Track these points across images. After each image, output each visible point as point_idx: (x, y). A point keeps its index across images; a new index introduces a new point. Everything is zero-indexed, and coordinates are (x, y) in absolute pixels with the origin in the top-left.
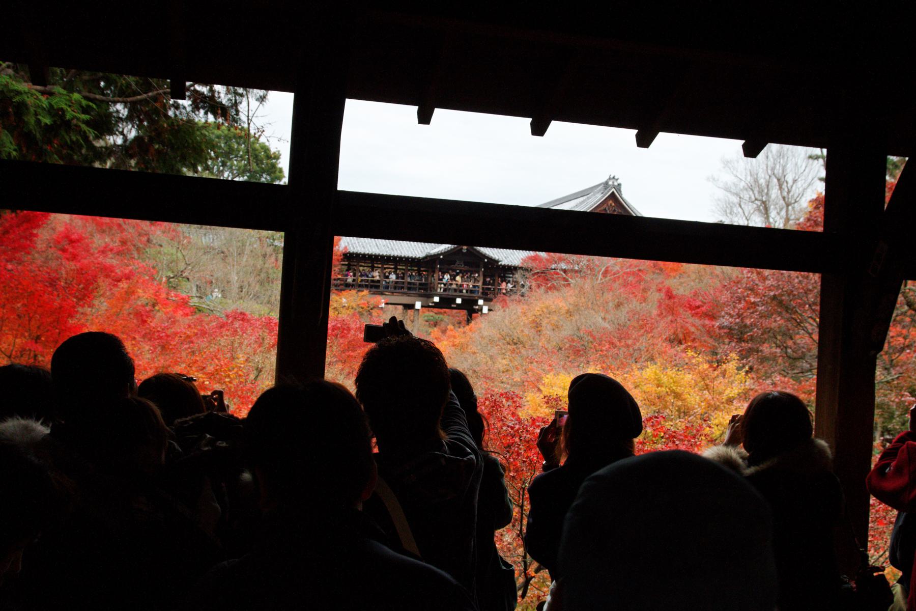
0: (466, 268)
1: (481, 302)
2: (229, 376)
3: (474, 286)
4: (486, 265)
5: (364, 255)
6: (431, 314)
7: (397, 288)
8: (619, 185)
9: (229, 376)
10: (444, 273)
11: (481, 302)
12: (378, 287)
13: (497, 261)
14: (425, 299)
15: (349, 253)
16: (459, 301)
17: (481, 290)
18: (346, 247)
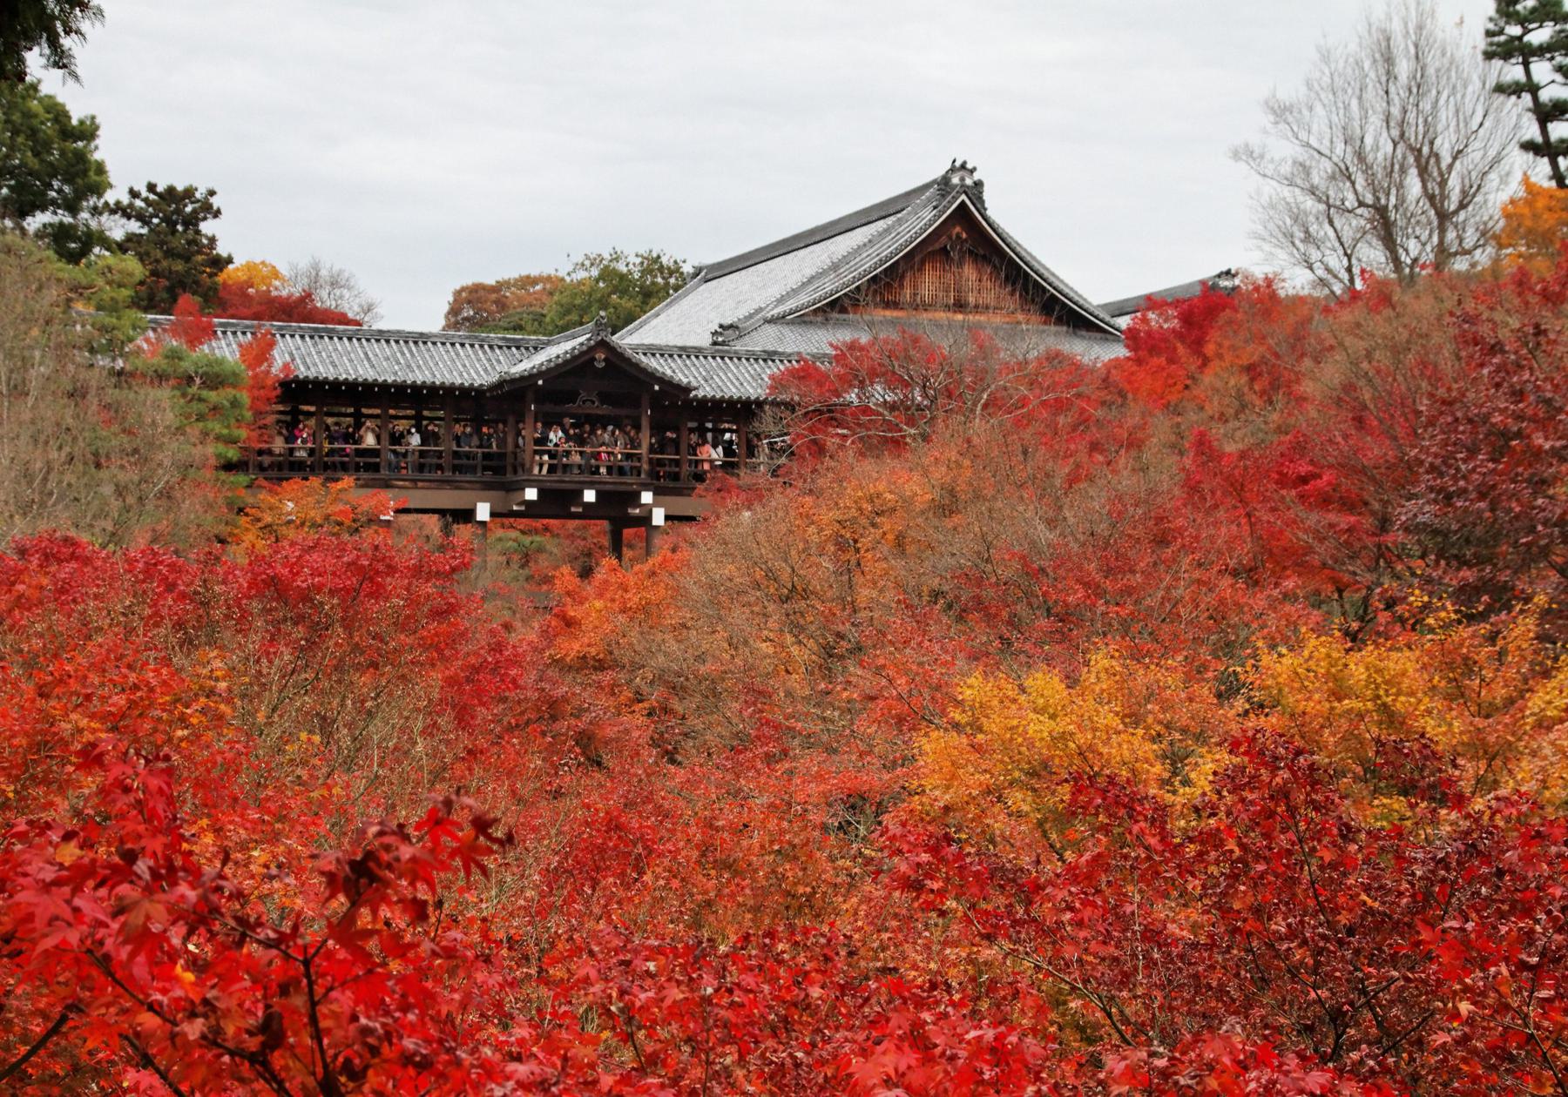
0: (605, 410)
1: (647, 497)
2: (183, 721)
3: (628, 457)
4: (656, 401)
5: (336, 384)
6: (514, 534)
7: (426, 467)
8: (979, 184)
9: (183, 721)
10: (548, 426)
11: (647, 497)
12: (375, 468)
13: (687, 389)
14: (498, 494)
15: (296, 380)
16: (590, 496)
17: (645, 466)
18: (286, 366)
